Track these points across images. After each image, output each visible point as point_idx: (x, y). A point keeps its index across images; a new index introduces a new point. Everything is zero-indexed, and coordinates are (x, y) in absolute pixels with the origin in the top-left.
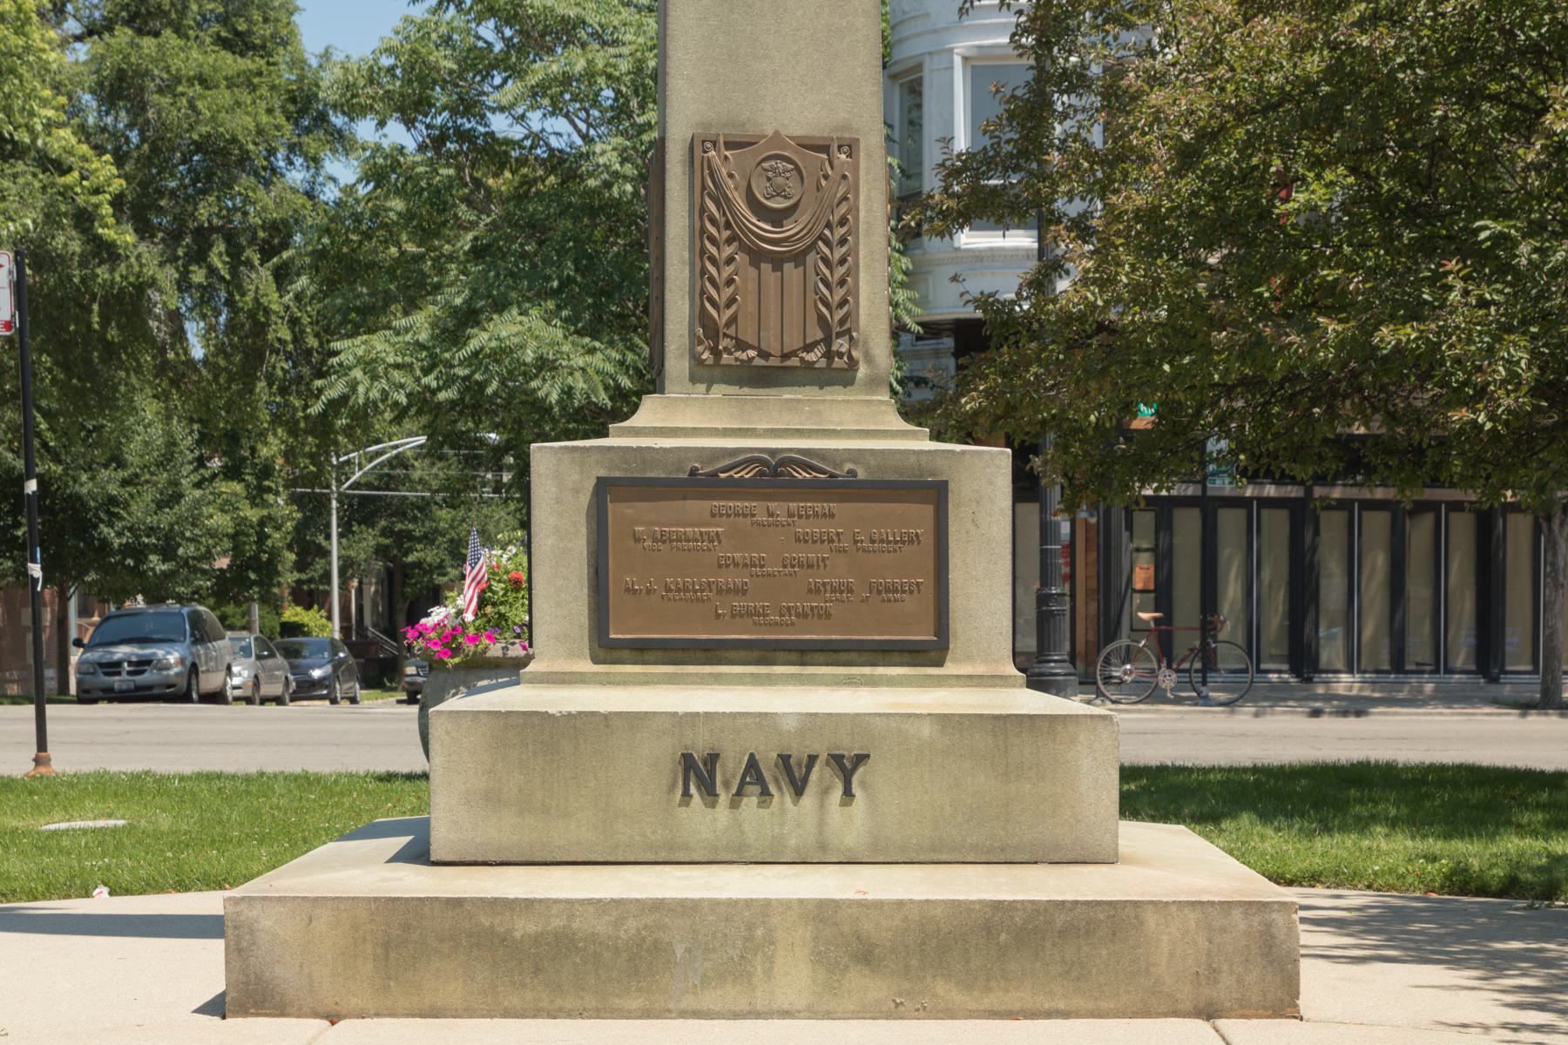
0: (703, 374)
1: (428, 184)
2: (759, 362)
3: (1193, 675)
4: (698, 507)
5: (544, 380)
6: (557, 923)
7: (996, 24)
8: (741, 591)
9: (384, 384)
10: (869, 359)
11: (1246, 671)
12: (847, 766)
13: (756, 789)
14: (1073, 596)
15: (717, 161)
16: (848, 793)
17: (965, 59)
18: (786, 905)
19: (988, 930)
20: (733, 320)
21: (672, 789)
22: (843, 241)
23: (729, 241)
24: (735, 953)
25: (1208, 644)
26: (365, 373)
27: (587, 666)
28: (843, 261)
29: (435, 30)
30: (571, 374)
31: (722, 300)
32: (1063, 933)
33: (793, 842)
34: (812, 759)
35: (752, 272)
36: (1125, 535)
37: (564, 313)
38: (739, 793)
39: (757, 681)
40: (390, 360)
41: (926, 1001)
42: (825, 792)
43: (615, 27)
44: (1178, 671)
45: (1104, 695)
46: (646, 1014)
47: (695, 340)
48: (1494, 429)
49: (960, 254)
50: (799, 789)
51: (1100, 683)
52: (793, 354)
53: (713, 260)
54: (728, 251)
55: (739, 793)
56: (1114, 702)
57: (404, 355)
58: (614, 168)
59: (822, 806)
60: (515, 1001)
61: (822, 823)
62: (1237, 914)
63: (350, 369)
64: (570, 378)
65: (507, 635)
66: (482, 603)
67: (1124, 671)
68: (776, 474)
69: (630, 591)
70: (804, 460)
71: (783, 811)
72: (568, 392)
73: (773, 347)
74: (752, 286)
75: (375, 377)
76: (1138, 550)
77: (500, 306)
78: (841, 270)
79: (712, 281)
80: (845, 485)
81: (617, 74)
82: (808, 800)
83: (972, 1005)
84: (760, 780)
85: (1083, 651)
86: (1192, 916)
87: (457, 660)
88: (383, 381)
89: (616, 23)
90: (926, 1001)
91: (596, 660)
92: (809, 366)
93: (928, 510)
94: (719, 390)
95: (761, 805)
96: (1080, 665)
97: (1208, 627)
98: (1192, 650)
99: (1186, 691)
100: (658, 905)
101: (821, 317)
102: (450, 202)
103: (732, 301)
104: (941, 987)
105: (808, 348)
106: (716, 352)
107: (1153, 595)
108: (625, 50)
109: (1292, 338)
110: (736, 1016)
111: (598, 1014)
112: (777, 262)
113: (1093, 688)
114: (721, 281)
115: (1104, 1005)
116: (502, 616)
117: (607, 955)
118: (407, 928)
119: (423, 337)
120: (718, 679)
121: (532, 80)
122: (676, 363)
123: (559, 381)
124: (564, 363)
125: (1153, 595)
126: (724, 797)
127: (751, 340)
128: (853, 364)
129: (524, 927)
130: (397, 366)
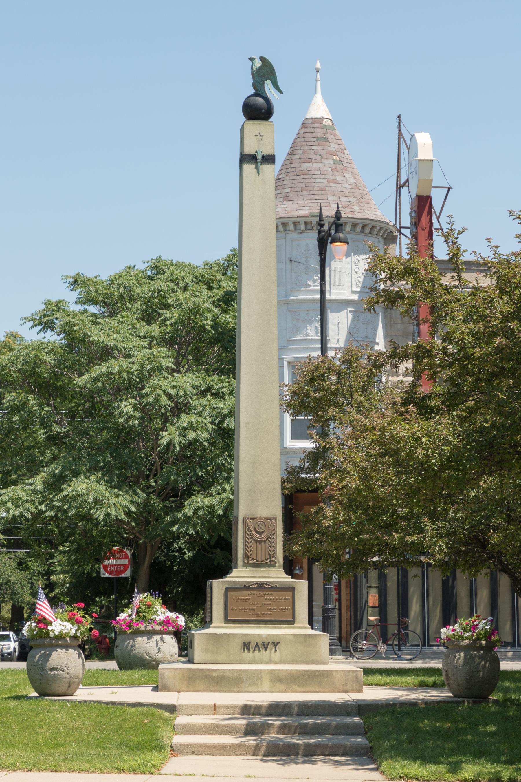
0: (245, 565)
1: (39, 415)
2: (257, 563)
3: (395, 647)
4: (246, 593)
5: (97, 509)
6: (221, 674)
7: (303, 348)
8: (254, 610)
9: (21, 509)
10: (279, 562)
11: (418, 645)
12: (275, 645)
13: (258, 649)
14: (340, 609)
15: (249, 522)
16: (276, 650)
17: (289, 363)
18: (265, 670)
19: (303, 675)
20: (251, 554)
21: (241, 649)
22: (274, 538)
23: (251, 538)
24: (255, 680)
25: (401, 632)
26: (13, 504)
27: (223, 625)
28: (273, 542)
29: (46, 348)
30: (109, 507)
31: (249, 550)
32: (318, 676)
33: (265, 660)
34: (269, 643)
35: (255, 544)
36: (364, 580)
37: (106, 478)
38: (254, 650)
39: (257, 628)
40: (25, 498)
41: (291, 689)
42: (271, 650)
43: (130, 348)
44: (388, 645)
45: (354, 656)
46: (238, 692)
47: (244, 558)
48: (435, 564)
49: (287, 450)
50: (266, 649)
51: (352, 650)
52: (263, 561)
53: (248, 542)
54: (251, 540)
55: (254, 650)
56: (358, 659)
57: (31, 496)
58: (130, 414)
59: (270, 653)
60: (213, 689)
61: (270, 656)
62: (351, 672)
63: (6, 502)
64: (109, 509)
65: (146, 622)
66: (138, 612)
67: (363, 644)
68: (261, 586)
69: (232, 610)
70: (267, 583)
71: (263, 653)
72: (108, 515)
73: (259, 559)
74: (255, 547)
75: (17, 506)
76: (370, 587)
77: (76, 474)
78: (273, 544)
79: (247, 546)
80: (275, 588)
81: (132, 370)
82: (268, 651)
83: (300, 690)
84: (258, 647)
85: (345, 635)
86: (342, 673)
87: (130, 631)
88: (21, 508)
89: (131, 346)
90: (291, 689)
91: (225, 623)
92: (267, 563)
93: (291, 593)
94: (248, 569)
95: (259, 652)
96: (344, 643)
97: (403, 625)
98: (393, 634)
99: (392, 655)
100: (240, 670)
101: (269, 553)
102: (50, 424)
103: (251, 550)
104: (294, 687)
105: (266, 560)
106: (248, 561)
107: (377, 609)
108: (134, 359)
109: (386, 538)
110: (255, 692)
111: (229, 691)
112: (260, 542)
113: (348, 653)
114: (249, 546)
115: (326, 690)
116: (144, 617)
117: (231, 680)
118: (193, 675)
119: (40, 487)
120: (249, 627)
121: (94, 375)
122: (240, 563)
123: (104, 510)
124: (106, 502)
125: (377, 609)
126: (251, 651)
127: (255, 558)
128: (275, 563)
129: (215, 674)
130: (27, 501)
